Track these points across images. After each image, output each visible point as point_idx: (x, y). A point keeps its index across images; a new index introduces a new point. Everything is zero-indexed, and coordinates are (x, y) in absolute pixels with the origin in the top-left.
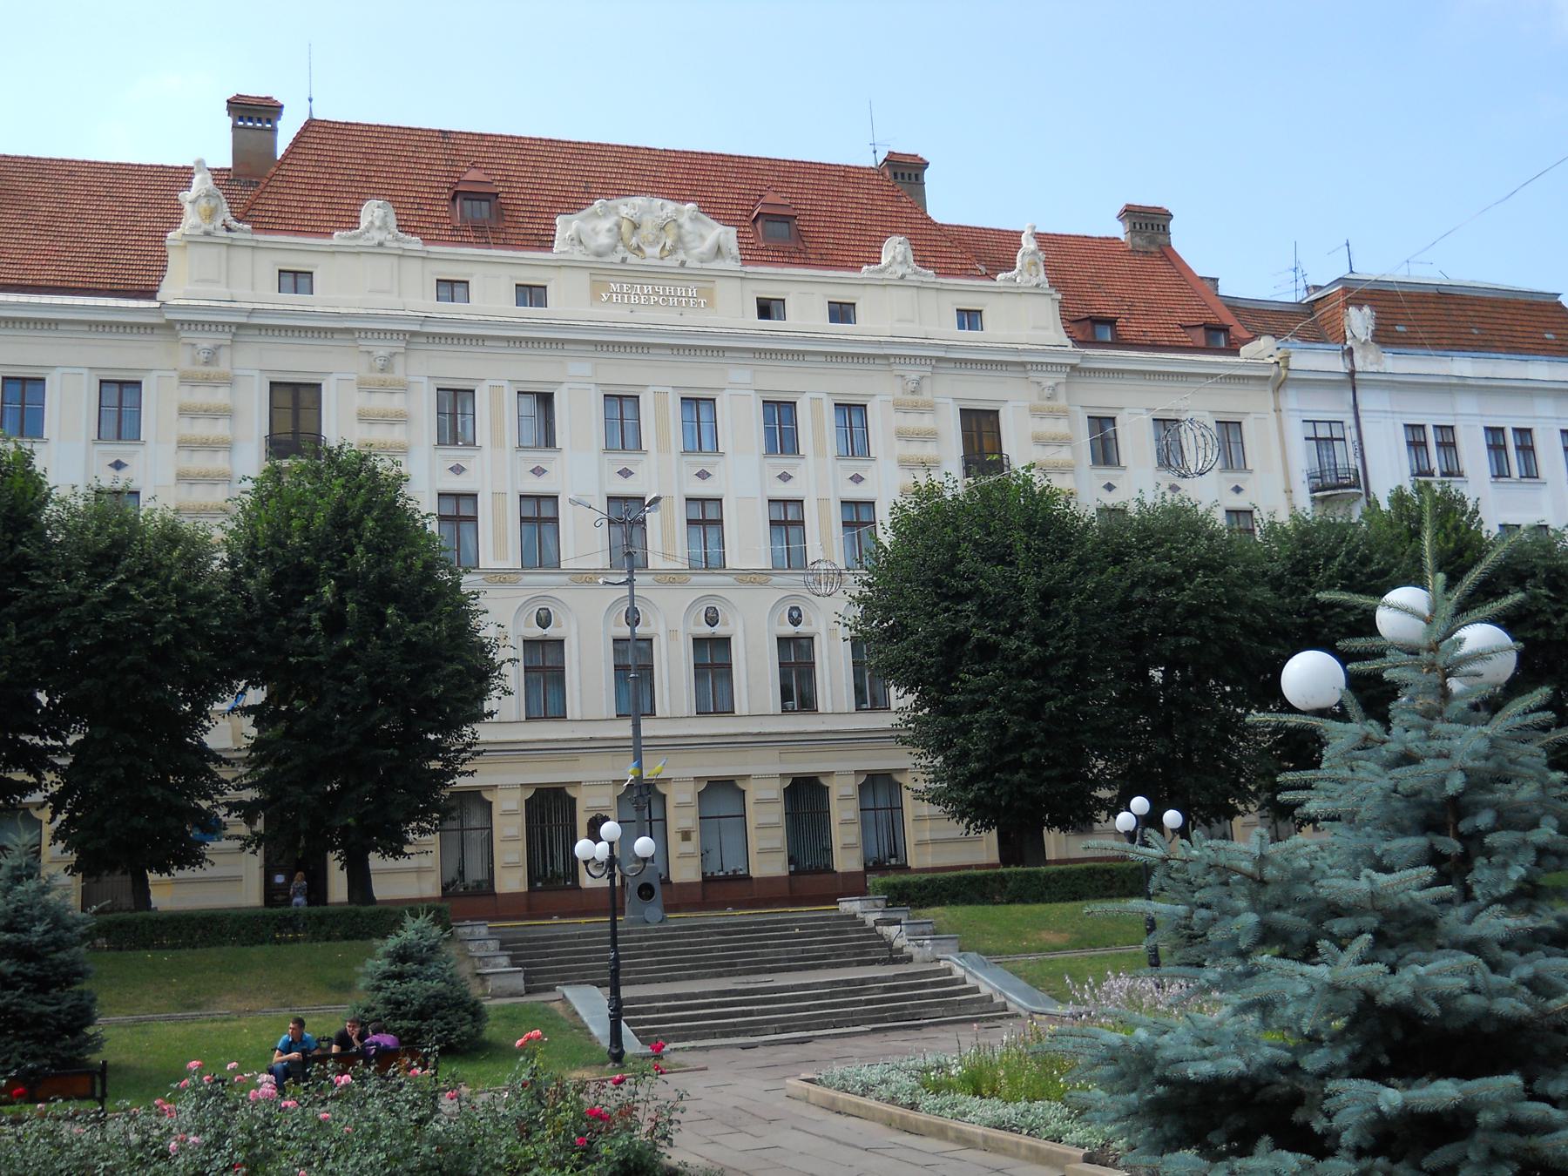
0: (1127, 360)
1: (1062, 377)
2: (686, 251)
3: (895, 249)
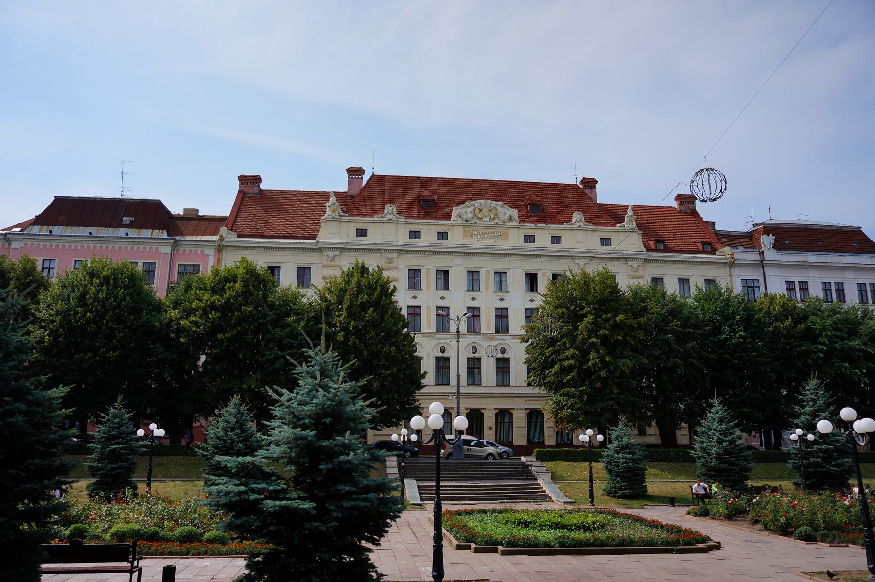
0: (660, 256)
1: (641, 263)
2: (499, 219)
3: (577, 216)
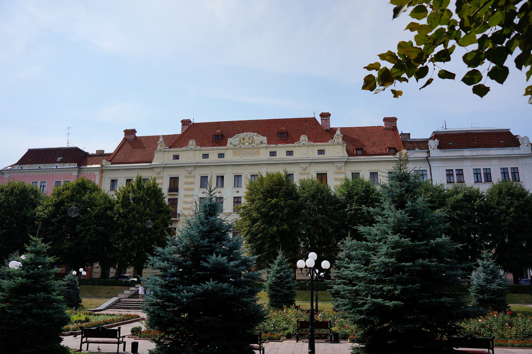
0: (360, 159)
3: (303, 138)
